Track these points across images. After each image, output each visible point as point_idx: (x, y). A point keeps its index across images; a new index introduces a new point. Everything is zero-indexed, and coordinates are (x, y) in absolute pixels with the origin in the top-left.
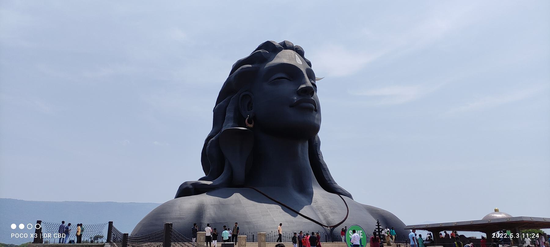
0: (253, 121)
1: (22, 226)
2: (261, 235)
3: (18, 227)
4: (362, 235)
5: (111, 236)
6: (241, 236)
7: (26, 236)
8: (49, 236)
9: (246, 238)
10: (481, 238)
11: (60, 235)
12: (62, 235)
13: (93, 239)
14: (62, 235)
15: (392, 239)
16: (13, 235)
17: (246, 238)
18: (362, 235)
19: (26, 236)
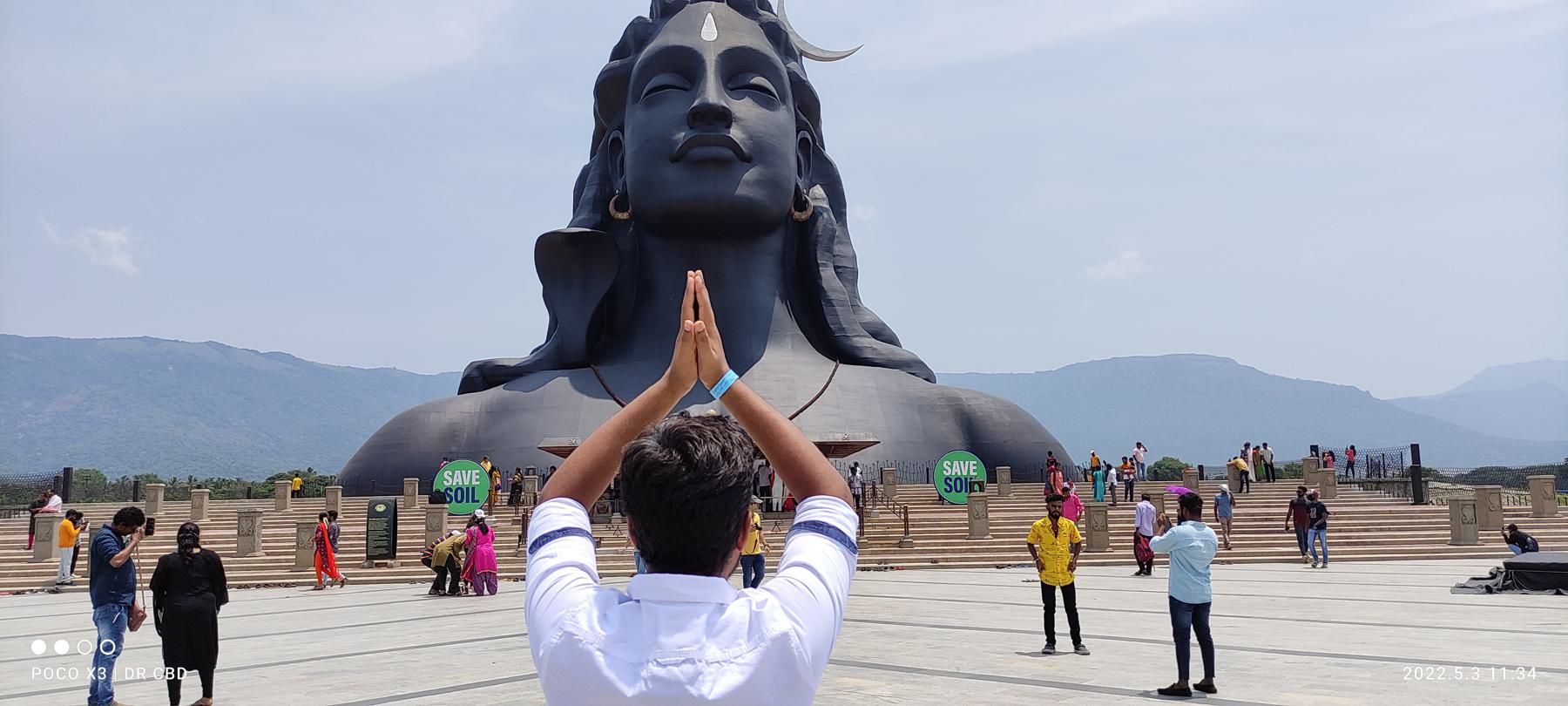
0: (161, 620)
1: (62, 647)
2: (1092, 509)
3: (50, 646)
4: (974, 471)
5: (1045, 494)
6: (1541, 476)
7: (73, 675)
8: (139, 674)
9: (1553, 481)
10: (1307, 454)
11: (172, 673)
12: (176, 673)
13: (712, 92)
14: (176, 673)
15: (1247, 462)
16: (36, 671)
17: (1553, 481)
18: (974, 471)
19: (73, 675)
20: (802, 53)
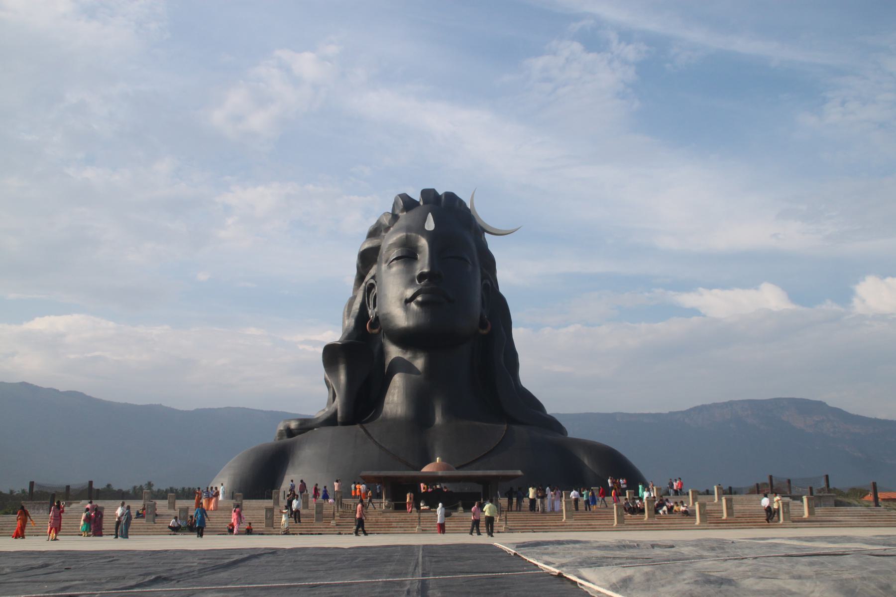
20: (484, 231)
